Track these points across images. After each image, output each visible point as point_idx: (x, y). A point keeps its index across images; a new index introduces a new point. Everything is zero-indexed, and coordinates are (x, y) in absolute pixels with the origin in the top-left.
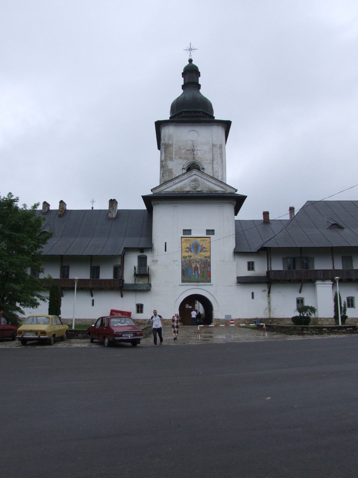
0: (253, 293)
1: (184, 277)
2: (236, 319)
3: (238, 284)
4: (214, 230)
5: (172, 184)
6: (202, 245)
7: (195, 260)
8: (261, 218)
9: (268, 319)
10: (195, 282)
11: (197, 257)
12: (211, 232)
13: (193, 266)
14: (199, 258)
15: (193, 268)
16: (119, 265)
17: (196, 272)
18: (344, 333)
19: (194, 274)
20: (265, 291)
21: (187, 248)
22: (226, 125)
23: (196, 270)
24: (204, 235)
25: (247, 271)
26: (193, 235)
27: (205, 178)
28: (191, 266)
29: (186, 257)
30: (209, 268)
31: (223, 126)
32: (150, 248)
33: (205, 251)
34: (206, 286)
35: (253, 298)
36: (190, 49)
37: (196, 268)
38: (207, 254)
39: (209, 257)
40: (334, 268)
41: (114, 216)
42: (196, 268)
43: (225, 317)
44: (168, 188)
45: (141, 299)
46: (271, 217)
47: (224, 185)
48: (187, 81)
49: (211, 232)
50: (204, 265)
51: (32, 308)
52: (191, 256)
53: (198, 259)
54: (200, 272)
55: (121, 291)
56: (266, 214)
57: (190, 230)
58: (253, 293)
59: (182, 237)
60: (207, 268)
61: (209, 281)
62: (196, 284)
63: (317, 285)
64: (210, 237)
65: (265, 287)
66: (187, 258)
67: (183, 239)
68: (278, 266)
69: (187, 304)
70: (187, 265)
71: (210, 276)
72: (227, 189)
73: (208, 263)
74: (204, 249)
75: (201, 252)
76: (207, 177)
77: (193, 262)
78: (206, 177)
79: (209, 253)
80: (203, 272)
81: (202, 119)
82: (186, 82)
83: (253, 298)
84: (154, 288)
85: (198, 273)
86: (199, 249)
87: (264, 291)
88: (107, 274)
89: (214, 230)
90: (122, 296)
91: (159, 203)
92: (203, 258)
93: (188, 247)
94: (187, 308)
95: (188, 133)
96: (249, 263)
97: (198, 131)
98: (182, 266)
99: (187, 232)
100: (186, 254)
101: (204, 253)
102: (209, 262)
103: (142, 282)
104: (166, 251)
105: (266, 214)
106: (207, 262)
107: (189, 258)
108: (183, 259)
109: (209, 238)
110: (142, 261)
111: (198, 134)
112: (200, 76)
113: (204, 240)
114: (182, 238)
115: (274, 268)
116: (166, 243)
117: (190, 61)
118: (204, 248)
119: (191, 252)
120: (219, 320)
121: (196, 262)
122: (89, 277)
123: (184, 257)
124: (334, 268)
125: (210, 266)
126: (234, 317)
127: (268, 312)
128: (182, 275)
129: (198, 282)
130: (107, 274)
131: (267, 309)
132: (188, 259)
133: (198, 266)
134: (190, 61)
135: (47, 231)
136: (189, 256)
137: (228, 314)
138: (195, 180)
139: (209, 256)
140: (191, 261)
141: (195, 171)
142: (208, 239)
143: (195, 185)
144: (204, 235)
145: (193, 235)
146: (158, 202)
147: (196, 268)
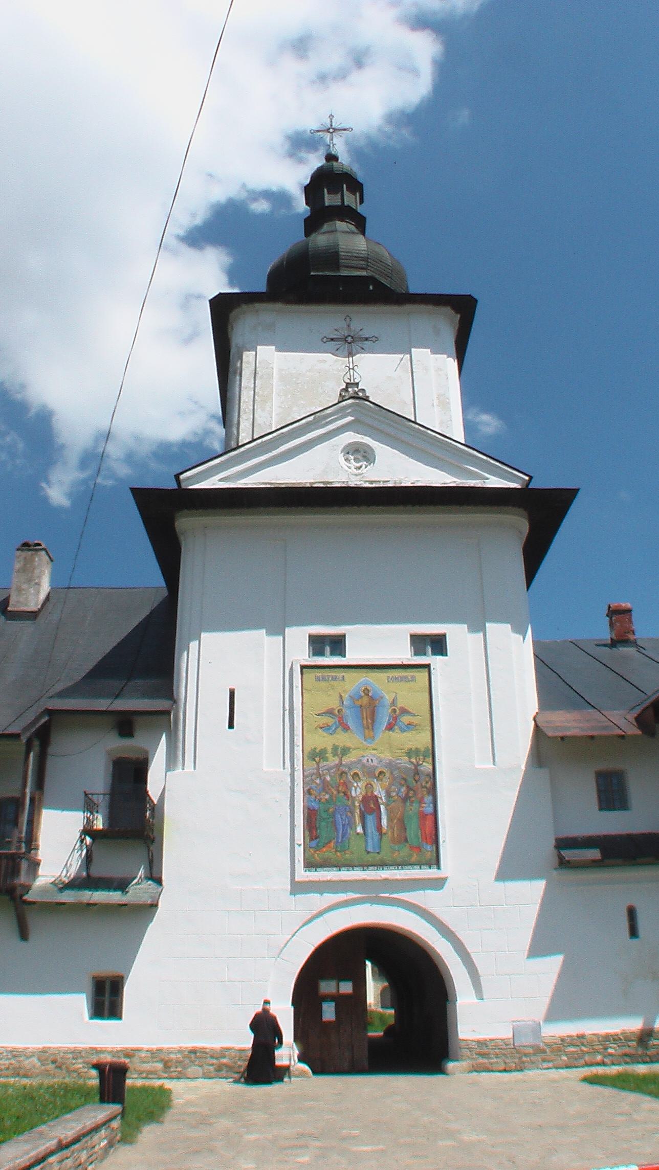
0: (632, 913)
1: (314, 843)
7: (364, 766)
13: (357, 791)
15: (357, 804)
17: (370, 819)
19: (359, 829)
21: (330, 712)
23: (371, 811)
26: (352, 656)
28: (345, 794)
30: (428, 799)
35: (634, 932)
37: (370, 804)
38: (420, 740)
52: (345, 751)
54: (390, 820)
58: (632, 913)
60: (421, 801)
64: (428, 666)
66: (326, 759)
70: (325, 786)
74: (406, 719)
75: (390, 727)
83: (634, 932)
85: (379, 827)
86: (384, 718)
90: (24, 935)
93: (333, 709)
100: (323, 741)
106: (417, 772)
114: (304, 670)
118: (404, 711)
119: (346, 728)
132: (333, 761)
133: (379, 791)
136: (335, 748)
139: (427, 749)
140: (343, 773)
145: (352, 656)
147: (370, 804)
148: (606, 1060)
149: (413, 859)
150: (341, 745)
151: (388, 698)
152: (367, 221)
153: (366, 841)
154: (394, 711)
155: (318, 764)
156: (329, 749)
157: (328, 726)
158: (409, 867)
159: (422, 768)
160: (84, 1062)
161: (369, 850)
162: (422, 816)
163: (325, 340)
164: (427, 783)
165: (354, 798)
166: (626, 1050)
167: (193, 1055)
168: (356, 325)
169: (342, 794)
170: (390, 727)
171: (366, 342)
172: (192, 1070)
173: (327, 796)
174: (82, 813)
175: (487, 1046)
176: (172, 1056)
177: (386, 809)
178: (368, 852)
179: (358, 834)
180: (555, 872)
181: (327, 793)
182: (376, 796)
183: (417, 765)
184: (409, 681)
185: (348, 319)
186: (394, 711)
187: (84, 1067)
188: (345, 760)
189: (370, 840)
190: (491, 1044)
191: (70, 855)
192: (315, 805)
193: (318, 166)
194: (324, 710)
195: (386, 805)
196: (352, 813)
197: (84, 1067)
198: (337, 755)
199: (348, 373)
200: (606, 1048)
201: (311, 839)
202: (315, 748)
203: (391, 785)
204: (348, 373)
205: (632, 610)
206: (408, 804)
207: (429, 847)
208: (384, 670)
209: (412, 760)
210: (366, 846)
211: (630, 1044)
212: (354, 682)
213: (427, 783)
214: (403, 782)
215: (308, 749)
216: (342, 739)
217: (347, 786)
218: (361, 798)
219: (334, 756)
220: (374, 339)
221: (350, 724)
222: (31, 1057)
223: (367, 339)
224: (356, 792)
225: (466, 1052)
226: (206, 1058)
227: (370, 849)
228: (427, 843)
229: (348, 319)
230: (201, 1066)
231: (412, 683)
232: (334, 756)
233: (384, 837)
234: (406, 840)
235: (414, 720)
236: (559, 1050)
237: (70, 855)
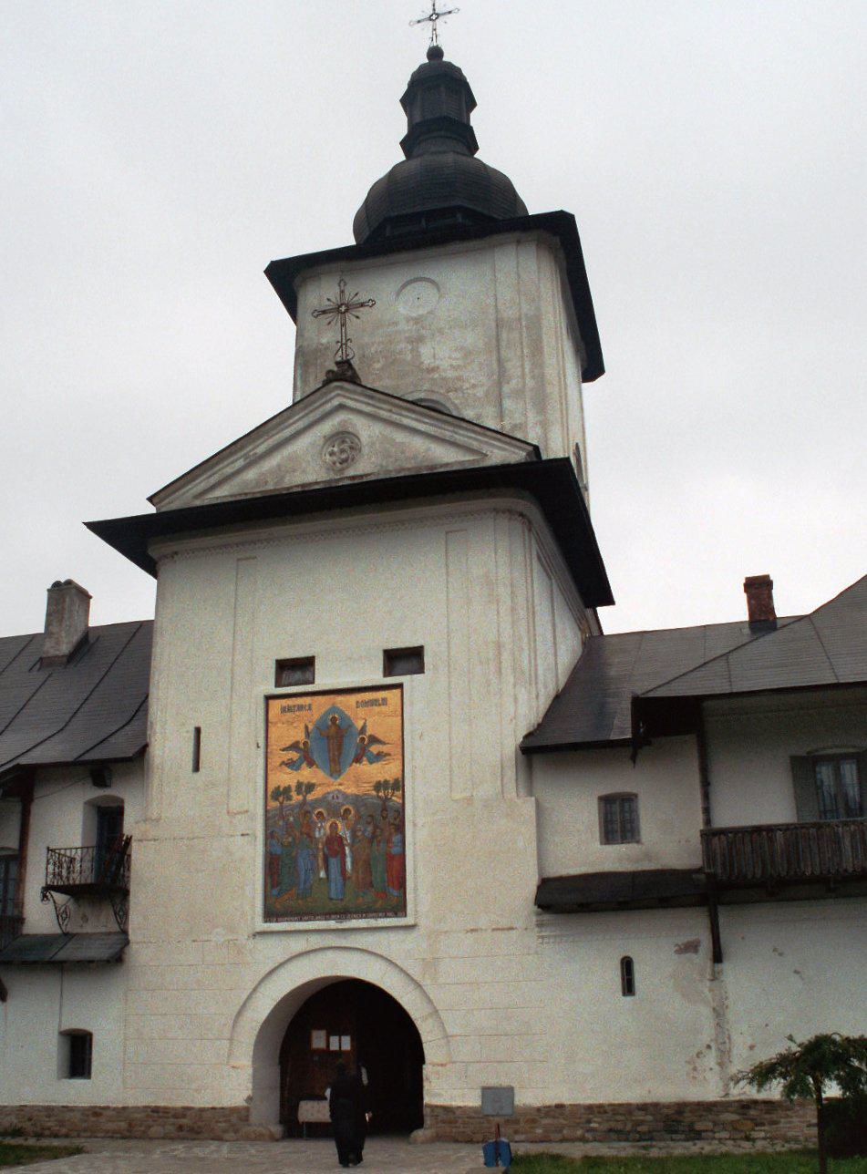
0: (627, 965)
1: (275, 892)
2: (538, 1110)
3: (546, 917)
4: (421, 648)
5: (240, 463)
6: (363, 730)
7: (329, 803)
8: (737, 610)
9: (715, 1104)
10: (327, 915)
11: (341, 787)
12: (404, 660)
13: (323, 830)
14: (349, 791)
15: (320, 846)
16: (10, 849)
17: (334, 862)
19: (322, 874)
20: (696, 951)
21: (295, 746)
22: (557, 240)
23: (335, 854)
25: (597, 844)
26: (323, 680)
27: (384, 414)
28: (309, 836)
29: (288, 789)
30: (396, 838)
31: (540, 244)
32: (136, 761)
33: (379, 757)
34: (382, 936)
35: (628, 987)
36: (434, 16)
37: (335, 844)
39: (399, 785)
41: (65, 649)
42: (336, 847)
43: (483, 1097)
46: (786, 605)
47: (474, 432)
48: (418, 119)
49: (404, 660)
50: (370, 829)
51: (756, 1088)
52: (310, 787)
53: (346, 796)
54: (353, 863)
56: (759, 589)
58: (627, 965)
59: (268, 698)
60: (388, 841)
61: (399, 908)
62: (332, 924)
64: (400, 686)
65: (695, 926)
66: (289, 798)
67: (276, 706)
69: (320, 1028)
71: (401, 884)
72: (485, 449)
73: (391, 815)
74: (374, 749)
75: (358, 760)
76: (394, 410)
77: (320, 814)
78: (390, 411)
79: (398, 763)
80: (365, 865)
81: (328, 397)
82: (414, 122)
83: (628, 987)
84: (140, 952)
87: (692, 947)
89: (421, 648)
91: (176, 553)
92: (367, 788)
93: (297, 743)
94: (319, 1051)
95: (398, 294)
96: (606, 801)
97: (433, 277)
98: (269, 835)
99: (295, 668)
100: (286, 778)
101: (374, 765)
102: (397, 811)
103: (99, 923)
104: (196, 768)
105: (759, 589)
106: (384, 809)
107: (301, 797)
108: (274, 804)
109: (397, 692)
110: (108, 821)
111: (439, 289)
112: (471, 104)
113: (374, 703)
114: (271, 702)
115: (728, 817)
116: (198, 731)
117: (435, 53)
118: (374, 740)
119: (311, 764)
120: (451, 1116)
121: (334, 811)
123: (278, 793)
125: (400, 828)
126: (527, 1098)
127: (717, 1068)
128: (269, 880)
129: (344, 913)
131: (709, 1047)
132: (296, 798)
133: (343, 831)
136: (299, 785)
137: (493, 1081)
139: (396, 781)
140: (307, 812)
141: (336, 392)
142: (392, 696)
143: (344, 456)
145: (323, 680)
146: (175, 548)
147: (335, 844)
148: (588, 1135)
149: (378, 906)
150: (306, 782)
151: (359, 724)
153: (329, 887)
154: (363, 739)
155: (281, 803)
156: (294, 789)
157: (293, 761)
158: (374, 914)
159: (391, 804)
160: (56, 1121)
161: (332, 896)
162: (390, 857)
163: (370, 304)
164: (395, 819)
165: (317, 841)
166: (613, 1124)
167: (155, 1115)
168: (350, 291)
169: (305, 836)
171: (361, 309)
172: (155, 1130)
173: (290, 839)
174: (79, 844)
175: (454, 1113)
176: (136, 1115)
177: (351, 851)
178: (331, 899)
179: (321, 879)
181: (290, 835)
182: (341, 837)
183: (387, 799)
184: (380, 705)
185: (342, 284)
186: (363, 739)
187: (56, 1126)
188: (310, 797)
189: (333, 885)
190: (458, 1113)
192: (278, 850)
194: (289, 743)
195: (351, 846)
196: (315, 857)
197: (56, 1126)
198: (302, 793)
199: (340, 352)
200: (589, 1121)
201: (273, 887)
202: (279, 787)
203: (357, 822)
204: (340, 352)
206: (375, 844)
207: (395, 893)
209: (380, 794)
210: (329, 893)
211: (618, 1117)
212: (322, 704)
213: (395, 819)
214: (369, 820)
215: (271, 787)
216: (306, 774)
217: (310, 826)
218: (324, 839)
219: (298, 794)
220: (370, 304)
221: (315, 757)
222: (10, 1114)
223: (362, 305)
224: (320, 833)
225: (428, 1121)
226: (168, 1118)
227: (333, 895)
228: (393, 887)
229: (342, 284)
230: (163, 1126)
231: (383, 707)
232: (298, 794)
233: (348, 883)
234: (371, 885)
235: (384, 749)
236: (534, 1121)
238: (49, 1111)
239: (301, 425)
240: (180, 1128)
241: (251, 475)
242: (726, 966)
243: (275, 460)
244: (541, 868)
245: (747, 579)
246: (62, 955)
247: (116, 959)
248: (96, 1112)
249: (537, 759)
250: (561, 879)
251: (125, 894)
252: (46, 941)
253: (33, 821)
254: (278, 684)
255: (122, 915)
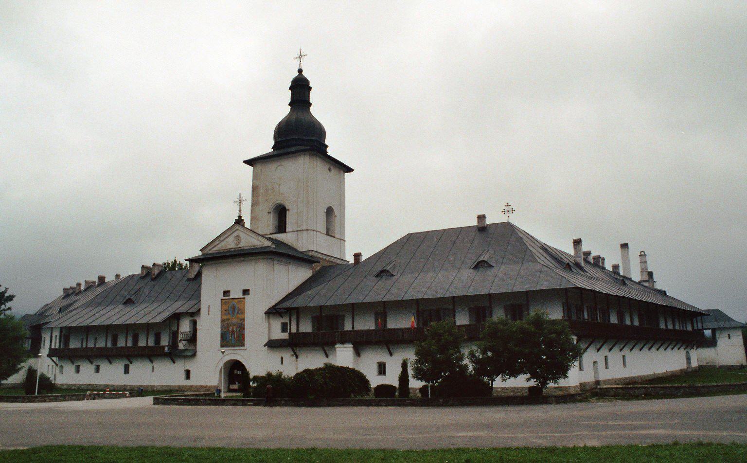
0: (282, 358)
5: (218, 242)
12: (246, 292)
17: (233, 335)
18: (176, 404)
24: (241, 296)
40: (353, 328)
41: (193, 276)
44: (213, 248)
45: (190, 365)
49: (246, 292)
55: (294, 351)
57: (229, 292)
58: (282, 358)
59: (222, 299)
61: (243, 345)
62: (232, 348)
63: (337, 349)
64: (245, 298)
68: (306, 327)
70: (225, 328)
72: (264, 242)
75: (238, 313)
81: (290, 150)
84: (199, 353)
88: (165, 341)
90: (391, 355)
98: (222, 329)
99: (226, 293)
100: (225, 317)
110: (194, 323)
117: (300, 71)
122: (131, 344)
124: (353, 328)
125: (244, 329)
129: (234, 346)
130: (165, 341)
133: (235, 330)
134: (300, 71)
135: (485, 259)
138: (238, 236)
144: (241, 296)
145: (231, 297)
147: (233, 331)
152: (191, 373)
170: (238, 313)
180: (361, 358)
191: (75, 309)
193: (657, 372)
205: (47, 355)
208: (219, 262)
216: (228, 317)
237: (75, 309)
238: (183, 386)
239: (230, 233)
240: (206, 390)
241: (220, 245)
242: (298, 360)
243: (225, 242)
244: (269, 337)
245: (385, 363)
246: (184, 354)
247: (194, 355)
248: (191, 386)
249: (271, 316)
250: (274, 340)
251: (196, 342)
252: (182, 351)
253: (180, 324)
254: (224, 296)
255: (195, 345)
